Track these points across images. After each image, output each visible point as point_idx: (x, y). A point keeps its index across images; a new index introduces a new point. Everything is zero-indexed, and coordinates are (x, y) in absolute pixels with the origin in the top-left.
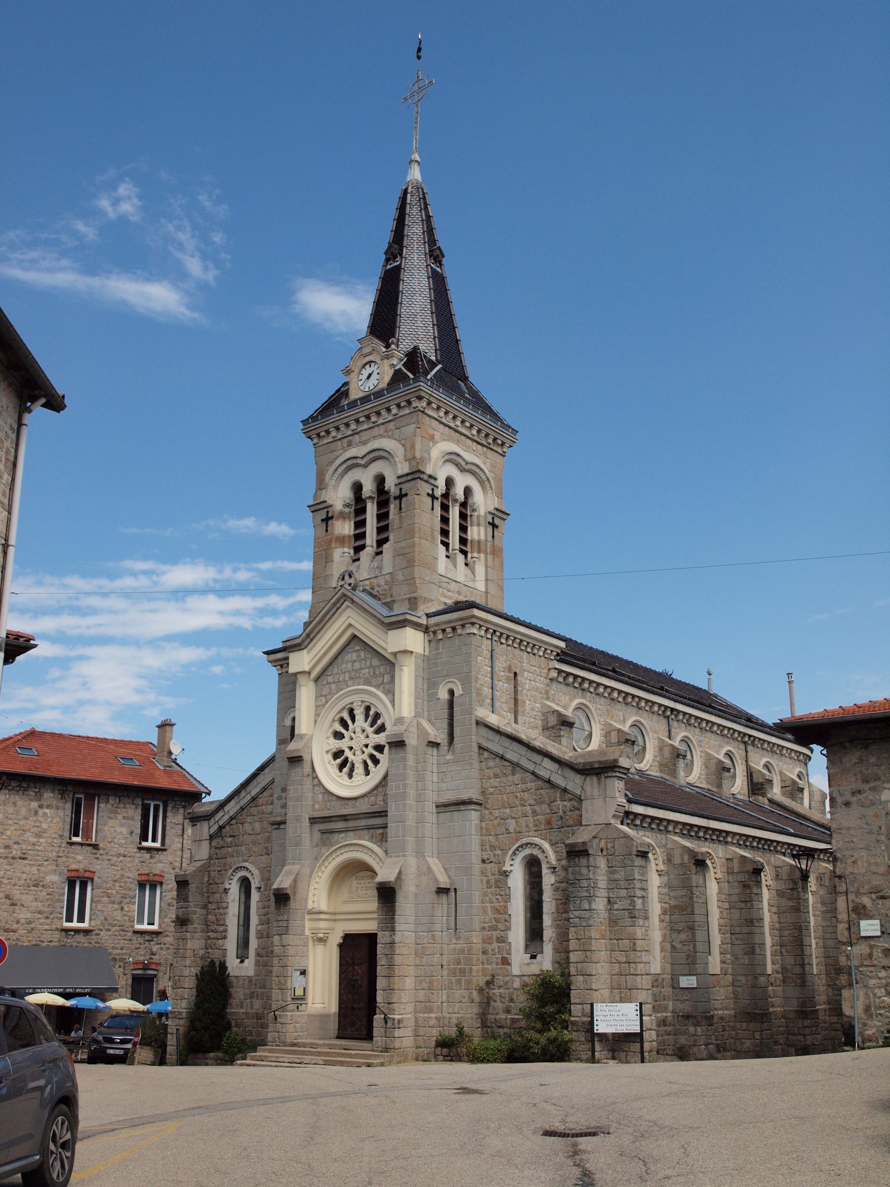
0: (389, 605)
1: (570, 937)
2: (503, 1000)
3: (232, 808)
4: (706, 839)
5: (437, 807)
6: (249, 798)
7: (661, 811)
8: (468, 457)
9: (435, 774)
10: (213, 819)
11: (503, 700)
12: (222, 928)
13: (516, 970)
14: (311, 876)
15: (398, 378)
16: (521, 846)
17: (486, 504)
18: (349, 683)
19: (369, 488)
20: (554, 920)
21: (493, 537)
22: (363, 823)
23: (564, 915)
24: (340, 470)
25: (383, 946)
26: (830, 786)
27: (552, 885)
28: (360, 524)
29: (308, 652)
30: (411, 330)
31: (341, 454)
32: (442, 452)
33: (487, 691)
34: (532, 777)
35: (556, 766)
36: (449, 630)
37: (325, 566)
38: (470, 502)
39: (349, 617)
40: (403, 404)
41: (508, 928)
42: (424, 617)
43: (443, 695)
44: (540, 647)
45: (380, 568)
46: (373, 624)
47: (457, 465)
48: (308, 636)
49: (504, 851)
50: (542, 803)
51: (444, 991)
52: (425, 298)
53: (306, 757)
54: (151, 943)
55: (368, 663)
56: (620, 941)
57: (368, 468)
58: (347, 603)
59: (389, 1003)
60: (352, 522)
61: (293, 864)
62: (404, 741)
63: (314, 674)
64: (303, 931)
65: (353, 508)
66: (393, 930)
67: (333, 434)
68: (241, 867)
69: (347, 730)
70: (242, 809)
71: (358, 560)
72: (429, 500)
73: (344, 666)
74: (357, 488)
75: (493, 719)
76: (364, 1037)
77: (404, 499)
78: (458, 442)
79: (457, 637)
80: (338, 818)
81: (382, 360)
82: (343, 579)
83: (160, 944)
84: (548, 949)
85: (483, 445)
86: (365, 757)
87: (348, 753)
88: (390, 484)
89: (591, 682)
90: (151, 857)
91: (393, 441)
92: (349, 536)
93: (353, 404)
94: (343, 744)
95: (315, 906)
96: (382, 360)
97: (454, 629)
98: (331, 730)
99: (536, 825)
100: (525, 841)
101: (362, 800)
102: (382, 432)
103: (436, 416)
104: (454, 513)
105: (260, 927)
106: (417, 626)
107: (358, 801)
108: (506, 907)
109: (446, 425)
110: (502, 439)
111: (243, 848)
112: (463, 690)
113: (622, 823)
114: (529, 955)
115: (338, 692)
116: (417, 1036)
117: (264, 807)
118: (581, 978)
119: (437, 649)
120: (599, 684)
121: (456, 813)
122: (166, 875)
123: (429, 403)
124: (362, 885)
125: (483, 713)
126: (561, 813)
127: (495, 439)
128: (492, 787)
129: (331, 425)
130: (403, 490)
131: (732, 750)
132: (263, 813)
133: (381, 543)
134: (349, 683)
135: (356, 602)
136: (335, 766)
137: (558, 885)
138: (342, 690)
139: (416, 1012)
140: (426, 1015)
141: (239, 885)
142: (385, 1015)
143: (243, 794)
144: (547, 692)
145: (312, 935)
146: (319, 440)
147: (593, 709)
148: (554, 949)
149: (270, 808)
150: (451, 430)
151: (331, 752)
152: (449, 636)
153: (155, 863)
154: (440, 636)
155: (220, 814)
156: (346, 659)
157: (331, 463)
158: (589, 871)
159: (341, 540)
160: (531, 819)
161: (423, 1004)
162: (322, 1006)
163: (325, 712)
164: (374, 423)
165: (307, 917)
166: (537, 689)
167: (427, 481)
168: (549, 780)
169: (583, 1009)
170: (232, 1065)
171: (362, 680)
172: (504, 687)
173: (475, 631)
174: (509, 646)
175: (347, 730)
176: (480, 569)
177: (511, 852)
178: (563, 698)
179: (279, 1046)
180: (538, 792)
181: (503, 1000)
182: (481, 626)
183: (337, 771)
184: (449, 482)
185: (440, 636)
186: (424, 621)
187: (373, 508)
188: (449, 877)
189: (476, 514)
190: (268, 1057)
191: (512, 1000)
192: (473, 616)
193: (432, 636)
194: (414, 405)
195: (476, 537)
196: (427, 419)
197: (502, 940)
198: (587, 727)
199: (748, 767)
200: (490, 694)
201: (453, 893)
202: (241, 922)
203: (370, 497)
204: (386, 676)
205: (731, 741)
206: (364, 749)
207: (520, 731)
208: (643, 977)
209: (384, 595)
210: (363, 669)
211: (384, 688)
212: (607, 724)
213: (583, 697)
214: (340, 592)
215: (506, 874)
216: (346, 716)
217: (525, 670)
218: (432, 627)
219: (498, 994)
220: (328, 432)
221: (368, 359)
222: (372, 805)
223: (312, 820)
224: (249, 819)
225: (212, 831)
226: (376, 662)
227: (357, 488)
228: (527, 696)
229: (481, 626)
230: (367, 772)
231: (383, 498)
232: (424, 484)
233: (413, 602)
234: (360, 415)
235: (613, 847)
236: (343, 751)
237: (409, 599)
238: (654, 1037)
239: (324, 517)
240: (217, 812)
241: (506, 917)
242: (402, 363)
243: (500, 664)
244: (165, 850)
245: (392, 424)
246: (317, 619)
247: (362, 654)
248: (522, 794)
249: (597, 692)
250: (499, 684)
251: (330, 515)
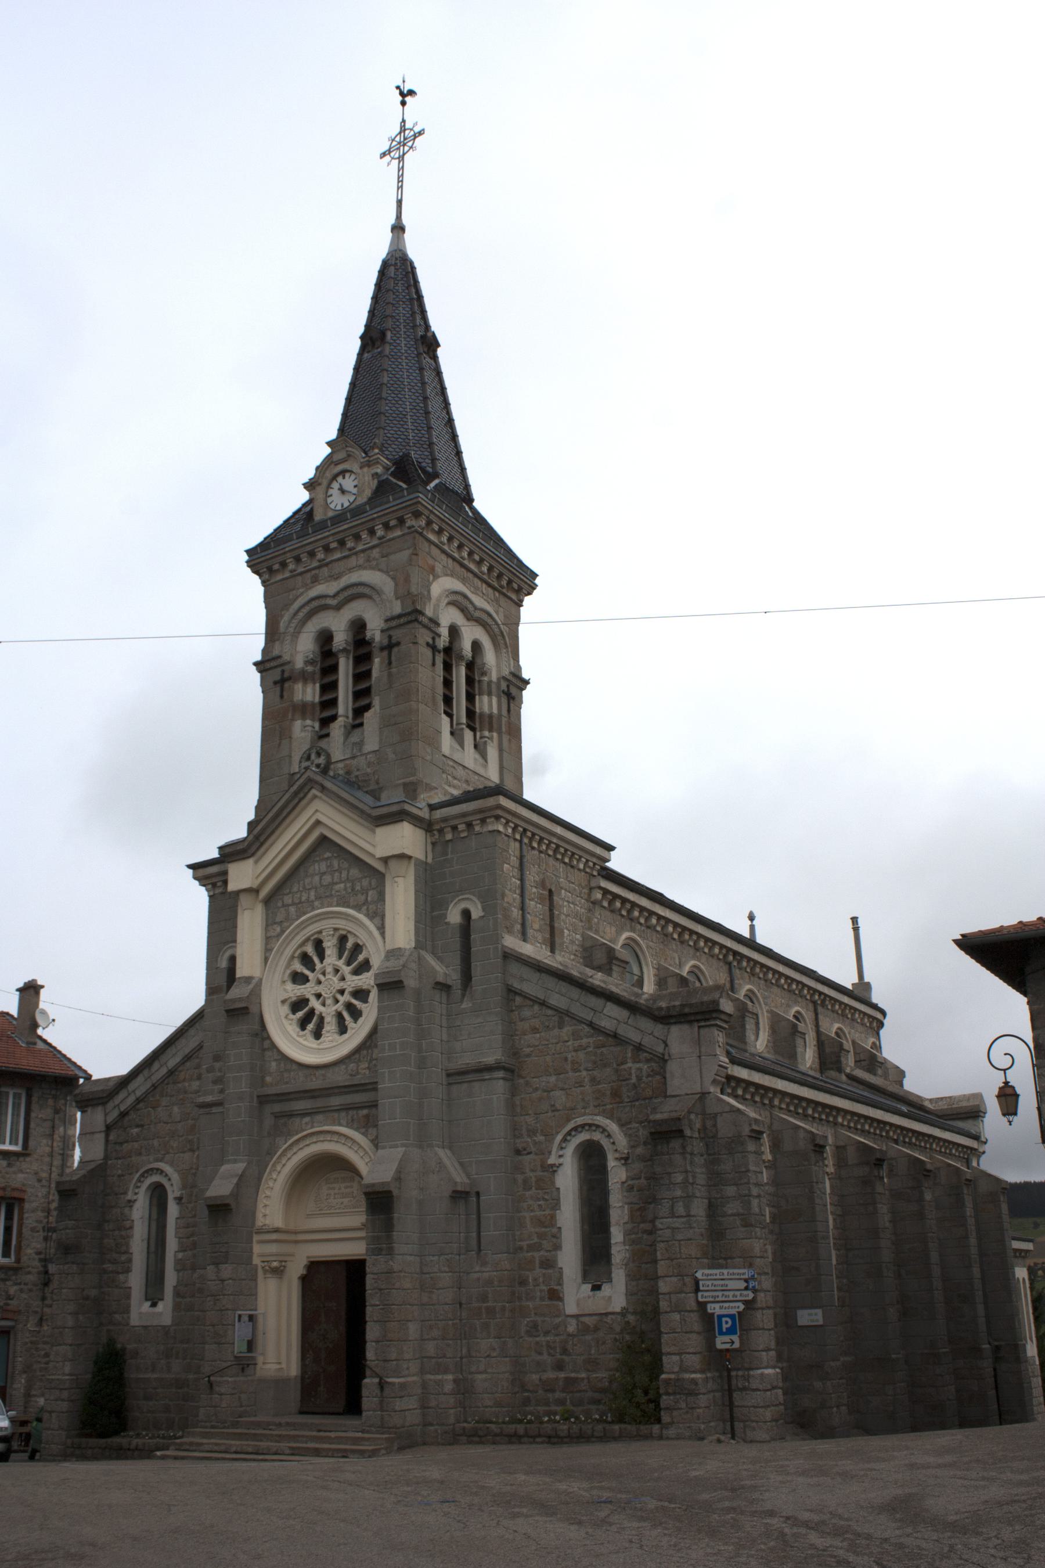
0: (375, 794)
1: (659, 1256)
2: (552, 1351)
3: (140, 1086)
4: (814, 1118)
5: (448, 1075)
6: (164, 1071)
7: (767, 1077)
8: (478, 601)
9: (444, 1030)
10: (111, 1101)
11: (536, 926)
12: (124, 1258)
13: (571, 1307)
14: (260, 1179)
15: (382, 489)
16: (575, 1129)
17: (498, 666)
18: (316, 903)
19: (340, 639)
20: (626, 1234)
21: (509, 711)
22: (336, 1101)
23: (642, 1225)
24: (301, 615)
25: (376, 1277)
26: (1034, 1028)
27: (623, 1183)
28: (329, 687)
29: (256, 862)
30: (399, 433)
31: (302, 594)
32: (448, 590)
33: (516, 913)
34: (587, 1029)
35: (624, 1013)
36: (462, 827)
37: (280, 745)
38: (478, 661)
39: (317, 811)
40: (392, 523)
41: (558, 1247)
42: (426, 810)
43: (454, 917)
44: (580, 857)
45: (360, 744)
46: (351, 818)
47: (463, 610)
48: (257, 837)
49: (549, 1136)
50: (605, 1066)
51: (464, 1341)
52: (417, 394)
53: (254, 1009)
54: (7, 1283)
55: (344, 875)
56: (729, 1261)
57: (342, 611)
58: (314, 791)
59: (385, 1361)
60: (318, 685)
61: (235, 1161)
62: (401, 982)
63: (263, 893)
64: (250, 1258)
65: (318, 667)
66: (390, 1252)
67: (291, 566)
68: (152, 1169)
69: (313, 970)
70: (154, 1087)
71: (327, 735)
72: (429, 653)
73: (307, 881)
74: (325, 638)
75: (527, 949)
76: (341, 1410)
77: (395, 650)
78: (464, 580)
79: (473, 836)
81: (361, 468)
82: (308, 758)
83: (20, 1284)
84: (619, 1276)
85: (494, 588)
86: (339, 1007)
87: (314, 1003)
88: (375, 628)
89: (642, 909)
90: (9, 1165)
91: (378, 573)
92: (313, 704)
93: (323, 525)
94: (307, 990)
95: (267, 1222)
96: (361, 468)
97: (469, 825)
98: (288, 972)
99: (597, 1098)
100: (580, 1121)
101: (336, 1069)
102: (361, 561)
103: (436, 541)
104: (460, 674)
105: (180, 1255)
106: (417, 821)
108: (553, 1217)
109: (448, 555)
110: (519, 582)
111: (156, 1143)
112: (484, 910)
113: (722, 1093)
114: (590, 1286)
115: (298, 918)
116: (425, 1408)
117: (187, 1084)
118: (676, 1316)
119: (445, 853)
120: (651, 913)
121: (477, 1085)
122: (29, 1190)
123: (429, 523)
124: (336, 1191)
125: (511, 942)
126: (634, 1080)
127: (510, 582)
128: (529, 1046)
129: (288, 555)
130: (394, 638)
131: (803, 1012)
132: (186, 1092)
133: (359, 712)
134: (316, 903)
135: (328, 789)
136: (295, 1022)
137: (630, 1182)
138: (305, 914)
139: (422, 1371)
140: (440, 1377)
141: (149, 1194)
142: (381, 1379)
143: (156, 1065)
144: (589, 920)
145: (263, 1264)
146: (270, 576)
147: (644, 946)
148: (627, 1275)
149: (195, 1085)
150: (455, 563)
151: (289, 1001)
152: (463, 835)
153: (14, 1173)
154: (449, 836)
155: (122, 1095)
156: (311, 871)
157: (286, 606)
158: (685, 1159)
159: (303, 710)
160: (588, 1088)
161: (434, 1360)
162: (278, 1366)
163: (281, 946)
164: (350, 550)
165: (255, 1238)
166: (576, 915)
167: (425, 626)
168: (616, 1033)
169: (682, 1361)
170: (149, 1458)
171: (335, 899)
172: (536, 908)
173: (501, 828)
174: (541, 852)
175: (322, 961)
176: (492, 752)
177: (559, 1137)
178: (608, 929)
180: (599, 1051)
181: (552, 1351)
182: (508, 822)
183: (298, 1029)
184: (454, 631)
185: (449, 836)
186: (425, 814)
187: (347, 665)
188: (468, 1176)
189: (486, 679)
190: (202, 1444)
191: (565, 1351)
192: (499, 807)
193: (437, 837)
194: (409, 523)
195: (486, 709)
196: (426, 544)
197: (549, 1264)
198: (636, 970)
199: (818, 1033)
200: (520, 917)
201: (474, 1199)
202: (152, 1249)
203: (344, 650)
204: (370, 893)
205: (800, 1000)
206: (339, 996)
207: (570, 966)
208: (764, 1312)
209: (365, 781)
210: (336, 883)
211: (368, 909)
212: (659, 968)
213: (633, 930)
214: (305, 776)
215: (553, 1169)
216: (310, 949)
217: (562, 888)
218: (438, 823)
219: (544, 1344)
220: (284, 565)
221: (340, 467)
222: (351, 1075)
224: (164, 1101)
225: (110, 1120)
226: (355, 872)
227: (325, 638)
228: (565, 923)
229: (508, 822)
230: (343, 1029)
231: (362, 651)
232: (423, 631)
233: (412, 790)
234: (331, 539)
235: (715, 1125)
236: (307, 1000)
237: (405, 785)
238: (781, 1398)
239: (278, 678)
240: (117, 1093)
241: (554, 1230)
242: (390, 472)
243: (532, 876)
244: (28, 1155)
245: (377, 550)
246: (271, 815)
247: (335, 863)
248: (574, 1054)
249: (648, 924)
250: (531, 905)
251: (286, 675)
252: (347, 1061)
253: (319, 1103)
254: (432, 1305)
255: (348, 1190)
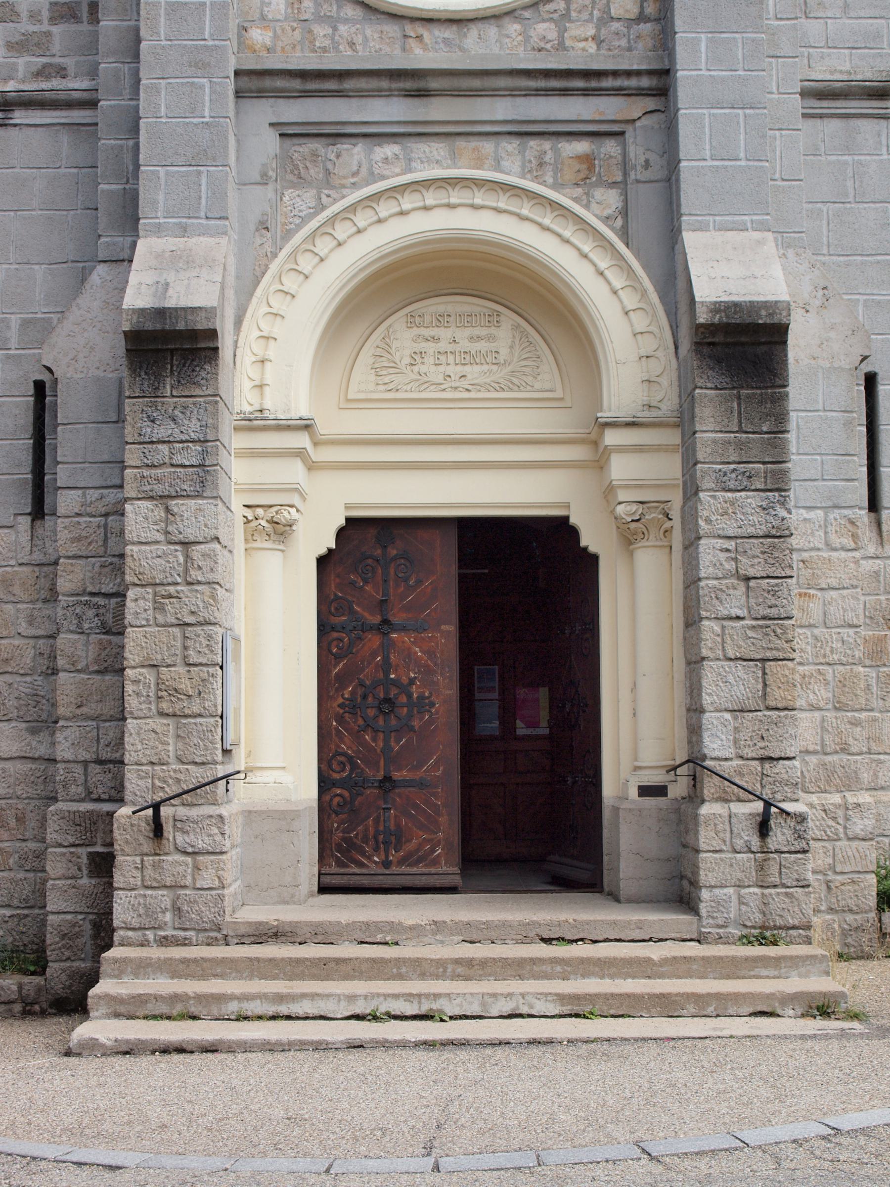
80: (385, 84)
107: (473, 32)
124: (443, 346)
179: (185, 943)
190: (221, 998)
223: (245, 82)
252: (527, 14)
253: (594, 84)
254: (810, 626)
255: (483, 346)
